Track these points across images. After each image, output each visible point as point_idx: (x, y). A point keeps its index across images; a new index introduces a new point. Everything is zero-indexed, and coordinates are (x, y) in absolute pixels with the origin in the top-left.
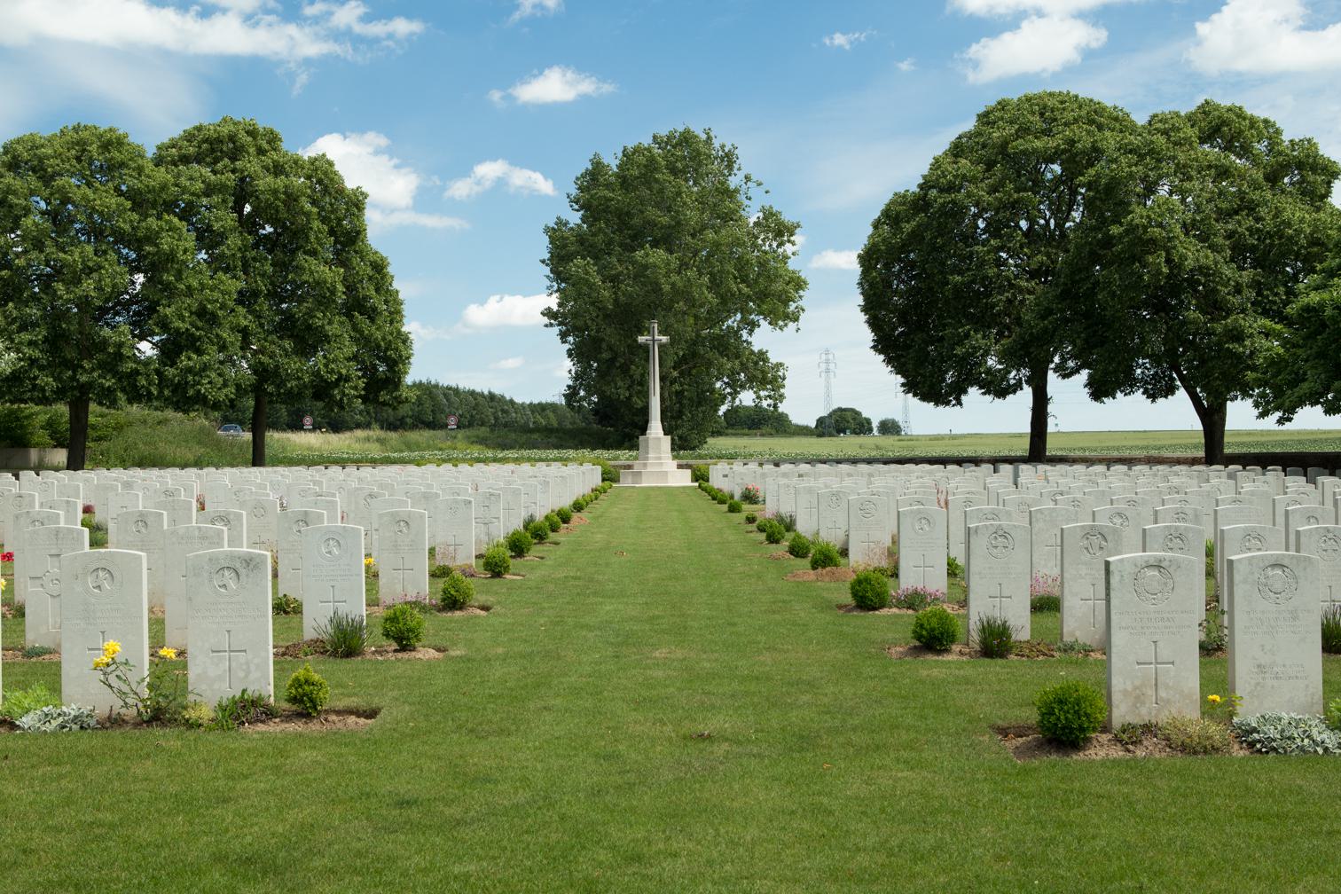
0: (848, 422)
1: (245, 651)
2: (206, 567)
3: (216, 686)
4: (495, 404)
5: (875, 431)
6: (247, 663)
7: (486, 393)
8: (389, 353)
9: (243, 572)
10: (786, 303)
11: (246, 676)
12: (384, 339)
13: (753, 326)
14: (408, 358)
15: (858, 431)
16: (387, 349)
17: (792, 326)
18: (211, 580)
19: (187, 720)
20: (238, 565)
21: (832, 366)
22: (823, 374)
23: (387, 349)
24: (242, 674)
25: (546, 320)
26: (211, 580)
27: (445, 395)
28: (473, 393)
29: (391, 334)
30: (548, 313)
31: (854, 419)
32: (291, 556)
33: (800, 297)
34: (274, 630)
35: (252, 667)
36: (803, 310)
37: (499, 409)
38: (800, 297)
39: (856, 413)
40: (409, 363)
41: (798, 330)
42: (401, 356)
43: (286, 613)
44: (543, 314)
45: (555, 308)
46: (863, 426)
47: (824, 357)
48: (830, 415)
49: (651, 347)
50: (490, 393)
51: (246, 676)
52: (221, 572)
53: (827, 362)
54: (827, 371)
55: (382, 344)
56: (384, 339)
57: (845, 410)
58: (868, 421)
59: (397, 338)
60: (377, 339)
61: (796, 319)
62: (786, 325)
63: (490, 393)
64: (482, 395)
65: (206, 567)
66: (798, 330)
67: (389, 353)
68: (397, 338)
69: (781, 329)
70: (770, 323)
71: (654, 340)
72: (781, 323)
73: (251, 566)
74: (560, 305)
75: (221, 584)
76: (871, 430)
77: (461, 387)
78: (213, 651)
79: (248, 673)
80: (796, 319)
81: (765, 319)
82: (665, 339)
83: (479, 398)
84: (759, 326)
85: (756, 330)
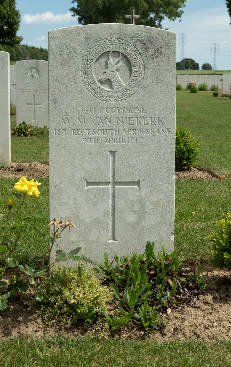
0: (189, 64)
1: (138, 183)
2: (81, 51)
3: (93, 236)
4: (43, 53)
5: (200, 68)
6: (141, 201)
7: (39, 48)
8: (10, 20)
9: (136, 60)
10: (177, 7)
11: (139, 222)
12: (7, 13)
13: (161, 18)
14: (18, 22)
15: (193, 68)
16: (8, 18)
17: (178, 19)
18: (87, 72)
19: (73, 307)
20: (129, 50)
21: (184, 40)
22: (181, 44)
23: (8, 18)
24: (131, 218)
25: (72, 13)
26: (87, 72)
27: (23, 49)
28: (33, 48)
29: (11, 11)
30: (73, 9)
31: (192, 63)
32: (26, 94)
33: (184, 6)
34: (11, 146)
35: (148, 207)
36: (183, 12)
37: (45, 55)
38: (184, 6)
39: (193, 61)
40: (19, 25)
41: (180, 21)
42: (15, 21)
43: (26, 135)
44: (70, 10)
45: (76, 7)
46: (195, 66)
47: (181, 36)
48: (182, 61)
49: (131, 20)
50: (41, 48)
51: (139, 222)
52: (104, 59)
53: (183, 38)
54: (183, 42)
55: (7, 15)
56: (7, 13)
57: (188, 59)
58: (197, 65)
59: (13, 13)
60: (4, 13)
61: (179, 16)
62: (175, 19)
63: (41, 48)
64: (38, 49)
65: (81, 51)
66: (180, 21)
67: (10, 20)
68: (13, 13)
69: (173, 20)
70: (169, 18)
71: (133, 17)
72: (173, 18)
73: (151, 52)
74: (78, 6)
75: (103, 77)
76: (198, 68)
77: (28, 45)
78: (89, 183)
79: (141, 215)
80: (179, 16)
81: (166, 15)
82: (137, 16)
83: (36, 50)
84: (164, 19)
85: (163, 21)
